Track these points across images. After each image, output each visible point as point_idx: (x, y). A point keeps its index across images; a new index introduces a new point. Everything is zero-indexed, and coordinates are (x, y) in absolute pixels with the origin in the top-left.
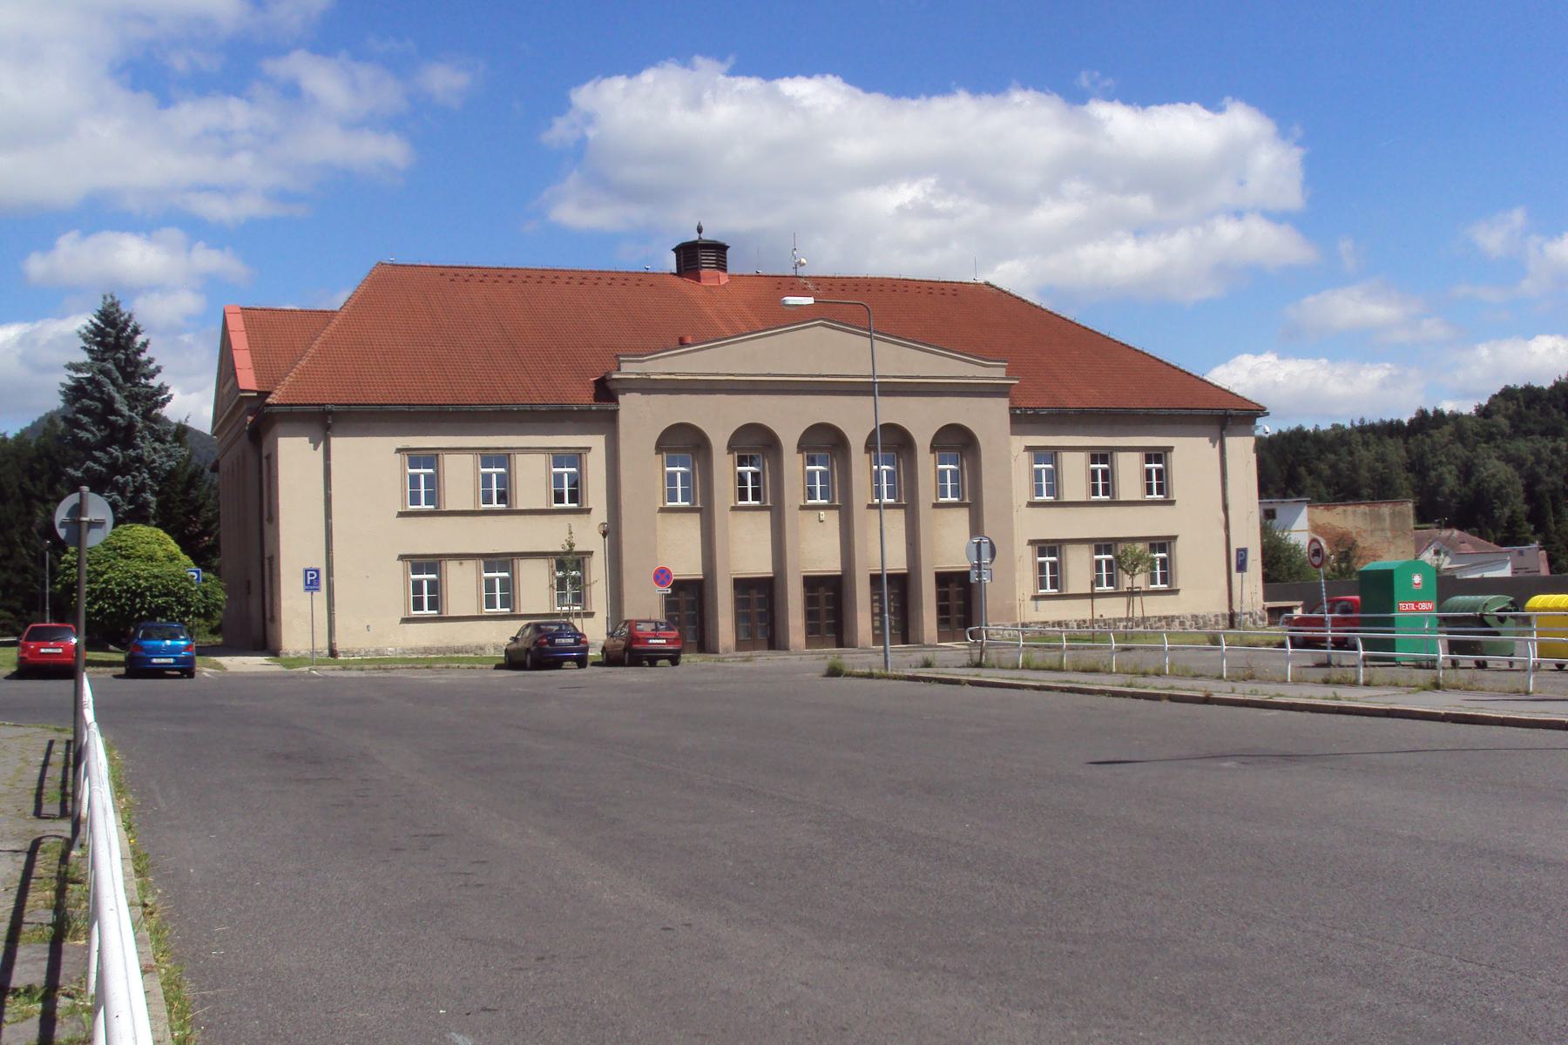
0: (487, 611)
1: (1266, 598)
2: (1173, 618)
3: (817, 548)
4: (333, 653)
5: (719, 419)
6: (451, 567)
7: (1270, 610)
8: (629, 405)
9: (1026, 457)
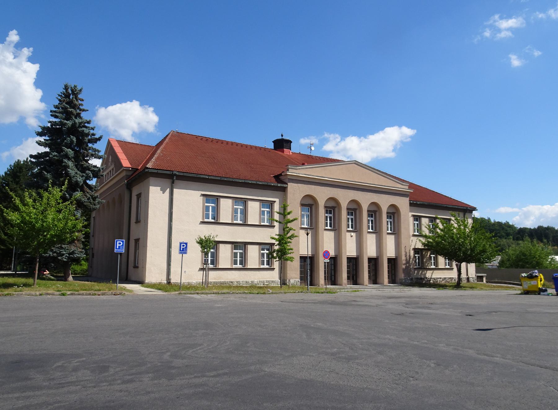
0: (234, 266)
1: (477, 272)
2: (453, 278)
3: (350, 249)
4: (169, 282)
5: (322, 195)
6: (250, 247)
7: (478, 277)
8: (291, 187)
9: (411, 219)
